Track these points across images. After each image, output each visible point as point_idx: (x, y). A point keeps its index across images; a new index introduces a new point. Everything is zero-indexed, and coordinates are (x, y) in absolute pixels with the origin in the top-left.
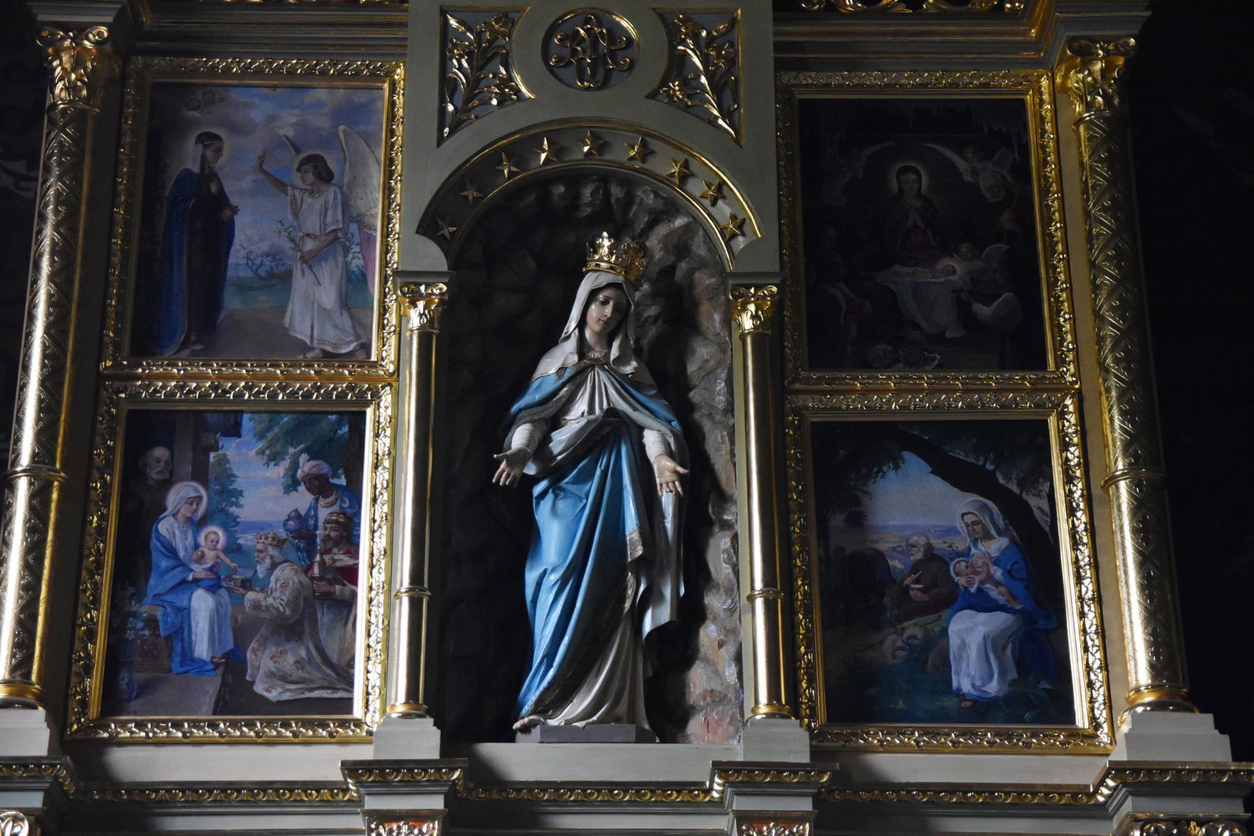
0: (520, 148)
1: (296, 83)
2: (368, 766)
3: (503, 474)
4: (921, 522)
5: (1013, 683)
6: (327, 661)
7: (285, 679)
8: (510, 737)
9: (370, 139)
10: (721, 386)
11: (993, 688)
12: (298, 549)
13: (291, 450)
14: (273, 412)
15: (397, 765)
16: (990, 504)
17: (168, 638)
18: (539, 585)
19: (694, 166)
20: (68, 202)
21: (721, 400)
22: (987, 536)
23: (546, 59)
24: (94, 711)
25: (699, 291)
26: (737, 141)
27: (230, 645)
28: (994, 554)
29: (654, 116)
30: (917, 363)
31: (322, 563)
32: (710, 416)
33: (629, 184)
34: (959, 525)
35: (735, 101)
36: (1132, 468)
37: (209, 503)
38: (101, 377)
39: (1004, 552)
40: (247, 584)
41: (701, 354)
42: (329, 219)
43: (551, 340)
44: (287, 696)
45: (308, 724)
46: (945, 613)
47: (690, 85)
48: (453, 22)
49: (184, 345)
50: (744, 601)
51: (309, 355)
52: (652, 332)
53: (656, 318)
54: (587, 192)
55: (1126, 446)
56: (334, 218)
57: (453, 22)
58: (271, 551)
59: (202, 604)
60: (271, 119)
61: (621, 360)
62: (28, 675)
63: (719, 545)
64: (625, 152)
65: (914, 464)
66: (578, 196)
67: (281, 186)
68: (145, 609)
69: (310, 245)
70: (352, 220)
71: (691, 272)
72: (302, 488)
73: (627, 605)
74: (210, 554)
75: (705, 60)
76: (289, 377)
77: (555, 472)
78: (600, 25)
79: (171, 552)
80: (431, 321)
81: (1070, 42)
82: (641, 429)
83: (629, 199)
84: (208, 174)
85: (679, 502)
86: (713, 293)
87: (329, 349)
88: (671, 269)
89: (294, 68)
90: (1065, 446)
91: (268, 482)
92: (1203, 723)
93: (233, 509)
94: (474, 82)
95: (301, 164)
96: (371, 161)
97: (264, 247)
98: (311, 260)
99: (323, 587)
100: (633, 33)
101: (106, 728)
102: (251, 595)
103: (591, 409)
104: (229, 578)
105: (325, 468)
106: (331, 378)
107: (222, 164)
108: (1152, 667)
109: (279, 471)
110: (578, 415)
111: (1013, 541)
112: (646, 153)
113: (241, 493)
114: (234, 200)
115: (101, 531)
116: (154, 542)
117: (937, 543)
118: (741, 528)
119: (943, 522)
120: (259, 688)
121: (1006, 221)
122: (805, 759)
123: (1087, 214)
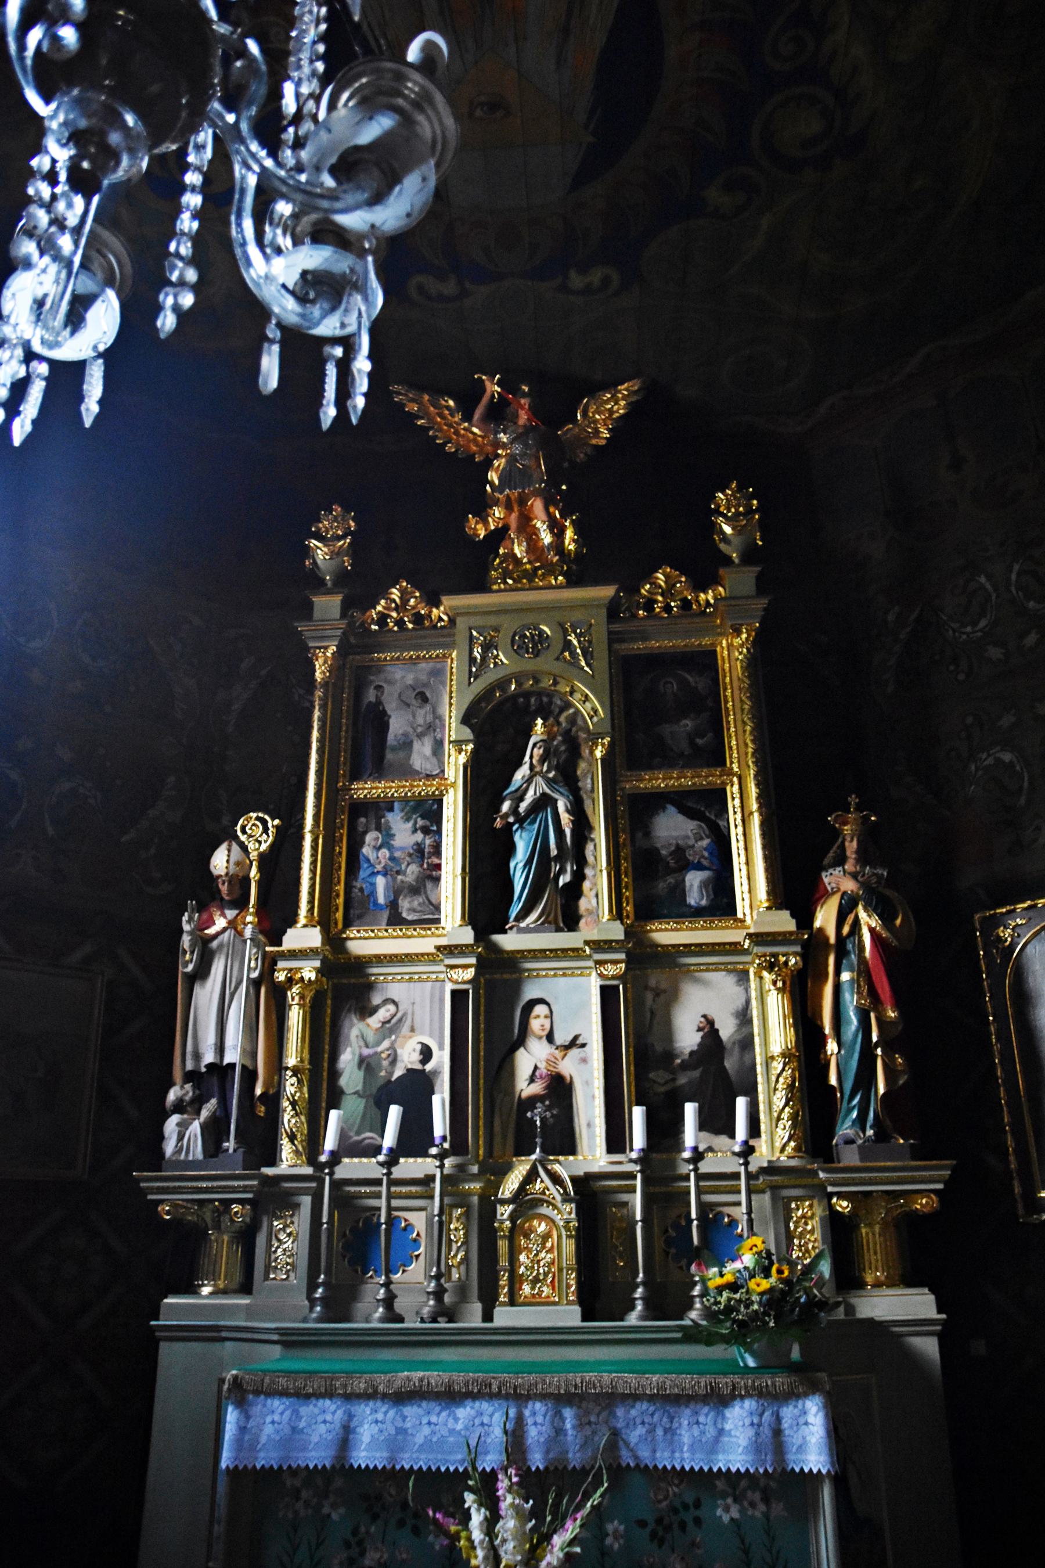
0: (502, 684)
1: (413, 661)
2: (445, 947)
3: (498, 823)
4: (674, 834)
5: (712, 900)
6: (431, 903)
7: (414, 910)
8: (505, 932)
9: (444, 684)
10: (589, 781)
11: (704, 902)
12: (418, 857)
13: (414, 816)
14: (405, 800)
15: (456, 946)
16: (703, 825)
17: (368, 896)
18: (515, 868)
19: (575, 688)
20: (322, 720)
21: (589, 786)
22: (702, 839)
23: (513, 646)
24: (340, 926)
25: (580, 740)
26: (593, 676)
27: (392, 898)
28: (705, 846)
29: (556, 667)
30: (672, 766)
31: (428, 863)
32: (586, 793)
33: (550, 695)
34: (690, 834)
35: (592, 659)
36: (760, 808)
37: (383, 839)
38: (338, 790)
39: (709, 845)
40: (398, 873)
41: (582, 766)
42: (428, 718)
43: (519, 764)
44: (415, 918)
45: (424, 929)
46: (684, 872)
47: (573, 654)
48: (475, 633)
49: (370, 775)
50: (598, 872)
51: (421, 776)
52: (563, 757)
53: (565, 751)
54: (533, 700)
55: (757, 798)
56: (430, 718)
57: (475, 633)
58: (408, 859)
59: (380, 882)
60: (403, 677)
61: (549, 771)
62: (313, 914)
63: (590, 847)
64: (547, 683)
65: (671, 809)
66: (529, 701)
67: (408, 705)
68: (358, 885)
69: (419, 730)
70: (437, 718)
71: (577, 731)
72: (419, 832)
73: (552, 875)
74: (383, 861)
75: (579, 642)
76: (412, 786)
77: (521, 820)
78: (535, 630)
79: (368, 860)
80: (467, 761)
81: (732, 627)
82: (556, 801)
83: (551, 703)
84: (379, 702)
85: (573, 831)
86: (586, 741)
87: (428, 773)
88: (570, 730)
89: (412, 656)
90: (733, 799)
91: (405, 830)
92: (785, 914)
93: (392, 842)
94: (484, 658)
95: (416, 695)
96: (444, 692)
97: (401, 732)
98: (420, 736)
99: (428, 872)
100: (549, 633)
101: (345, 933)
102: (399, 877)
103: (535, 793)
104: (391, 870)
105: (428, 823)
106: (429, 786)
107: (385, 698)
108: (768, 893)
109: (410, 825)
110: (530, 797)
111: (712, 841)
112: (555, 683)
113: (395, 835)
114: (389, 712)
115: (340, 853)
116: (361, 857)
117: (680, 842)
118: (597, 841)
119: (683, 833)
120: (404, 915)
121: (710, 703)
122: (622, 937)
123: (741, 698)
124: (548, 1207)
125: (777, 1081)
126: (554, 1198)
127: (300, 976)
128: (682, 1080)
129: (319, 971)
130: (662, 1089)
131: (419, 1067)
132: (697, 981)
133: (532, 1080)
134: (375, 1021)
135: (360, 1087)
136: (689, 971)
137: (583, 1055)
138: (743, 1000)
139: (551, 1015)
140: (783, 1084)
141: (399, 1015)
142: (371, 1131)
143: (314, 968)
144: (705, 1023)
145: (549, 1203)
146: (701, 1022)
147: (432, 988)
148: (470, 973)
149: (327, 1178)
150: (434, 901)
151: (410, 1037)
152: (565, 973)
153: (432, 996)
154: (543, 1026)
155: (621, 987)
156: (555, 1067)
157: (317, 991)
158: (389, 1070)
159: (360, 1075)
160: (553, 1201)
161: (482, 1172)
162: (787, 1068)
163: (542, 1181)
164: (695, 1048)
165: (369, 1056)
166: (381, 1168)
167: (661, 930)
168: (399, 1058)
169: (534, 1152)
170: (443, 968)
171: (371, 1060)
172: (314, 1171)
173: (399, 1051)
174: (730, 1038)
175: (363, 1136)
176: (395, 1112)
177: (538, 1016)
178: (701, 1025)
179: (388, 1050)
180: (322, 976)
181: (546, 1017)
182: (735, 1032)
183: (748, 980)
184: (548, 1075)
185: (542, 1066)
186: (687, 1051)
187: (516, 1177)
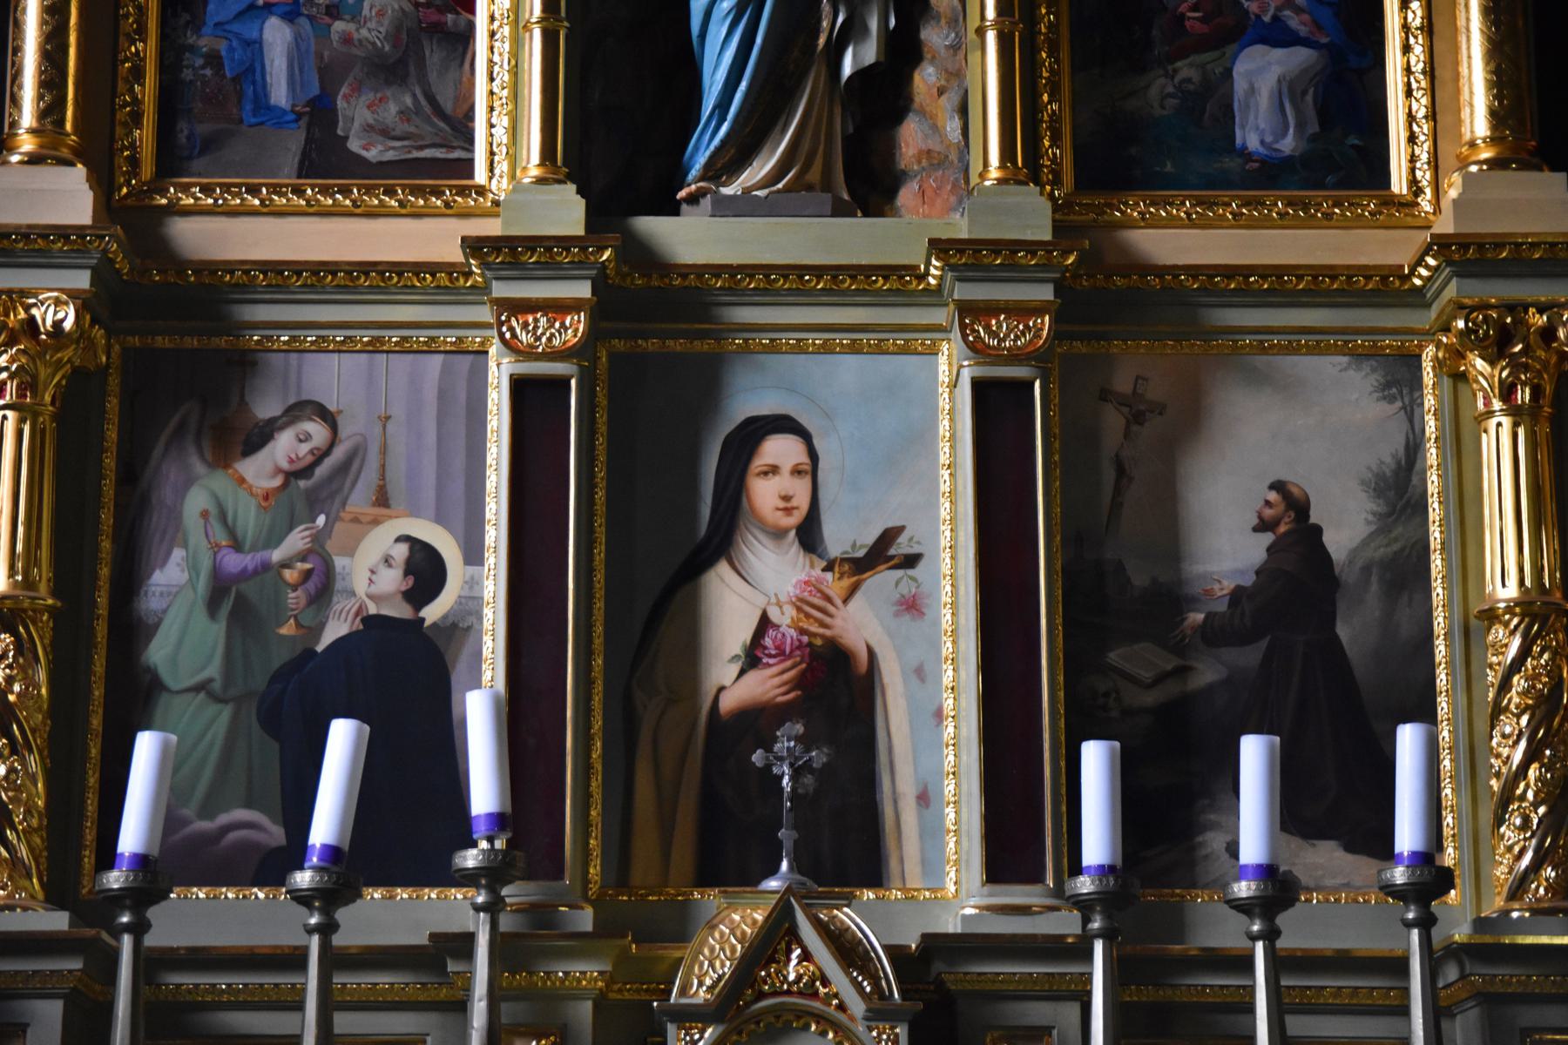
2: (496, 244)
7: (386, 133)
8: (673, 209)
11: (1288, 145)
15: (532, 243)
24: (147, 170)
44: (390, 156)
46: (1230, 49)
73: (822, 41)
102: (339, 26)
120: (354, 145)
124: (823, 1034)
125: (1505, 685)
126: (842, 1007)
127: (22, 315)
128: (1207, 673)
129: (84, 303)
130: (1149, 699)
131: (401, 611)
132: (1258, 379)
133: (752, 658)
134: (260, 470)
135: (213, 670)
136: (1236, 350)
137: (906, 589)
138: (1397, 443)
139: (812, 468)
140: (1524, 693)
141: (339, 453)
142: (248, 805)
143: (73, 295)
144: (1282, 507)
145: (825, 1022)
146: (1268, 503)
147: (446, 371)
148: (575, 328)
149: (127, 941)
150: (447, 105)
151: (376, 522)
152: (859, 341)
153: (443, 395)
154: (786, 498)
155: (1037, 384)
156: (823, 625)
157: (76, 371)
158: (307, 620)
159: (215, 632)
160: (841, 1016)
161: (606, 929)
162: (1536, 649)
163: (806, 956)
164: (1249, 580)
165: (244, 575)
166: (303, 910)
167: (1156, 223)
168: (339, 585)
169: (773, 871)
170: (485, 314)
171: (249, 588)
172: (71, 925)
173: (339, 562)
174: (1354, 553)
175: (224, 819)
176: (342, 737)
177: (773, 470)
178: (1268, 512)
179: (303, 557)
180: (94, 322)
181: (797, 472)
182: (1372, 536)
183: (1416, 383)
184: (800, 646)
185: (784, 617)
186: (1229, 585)
187: (723, 940)
